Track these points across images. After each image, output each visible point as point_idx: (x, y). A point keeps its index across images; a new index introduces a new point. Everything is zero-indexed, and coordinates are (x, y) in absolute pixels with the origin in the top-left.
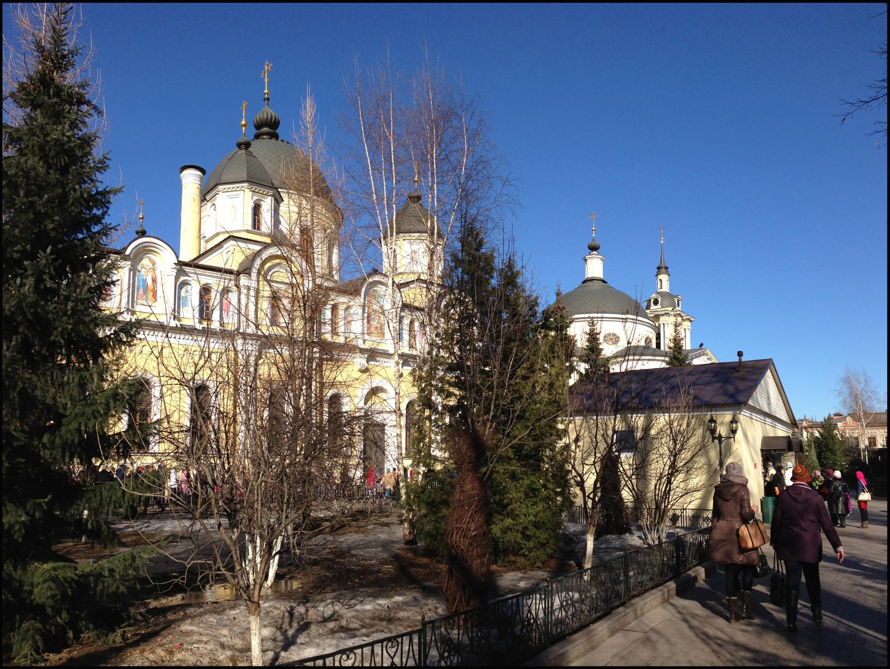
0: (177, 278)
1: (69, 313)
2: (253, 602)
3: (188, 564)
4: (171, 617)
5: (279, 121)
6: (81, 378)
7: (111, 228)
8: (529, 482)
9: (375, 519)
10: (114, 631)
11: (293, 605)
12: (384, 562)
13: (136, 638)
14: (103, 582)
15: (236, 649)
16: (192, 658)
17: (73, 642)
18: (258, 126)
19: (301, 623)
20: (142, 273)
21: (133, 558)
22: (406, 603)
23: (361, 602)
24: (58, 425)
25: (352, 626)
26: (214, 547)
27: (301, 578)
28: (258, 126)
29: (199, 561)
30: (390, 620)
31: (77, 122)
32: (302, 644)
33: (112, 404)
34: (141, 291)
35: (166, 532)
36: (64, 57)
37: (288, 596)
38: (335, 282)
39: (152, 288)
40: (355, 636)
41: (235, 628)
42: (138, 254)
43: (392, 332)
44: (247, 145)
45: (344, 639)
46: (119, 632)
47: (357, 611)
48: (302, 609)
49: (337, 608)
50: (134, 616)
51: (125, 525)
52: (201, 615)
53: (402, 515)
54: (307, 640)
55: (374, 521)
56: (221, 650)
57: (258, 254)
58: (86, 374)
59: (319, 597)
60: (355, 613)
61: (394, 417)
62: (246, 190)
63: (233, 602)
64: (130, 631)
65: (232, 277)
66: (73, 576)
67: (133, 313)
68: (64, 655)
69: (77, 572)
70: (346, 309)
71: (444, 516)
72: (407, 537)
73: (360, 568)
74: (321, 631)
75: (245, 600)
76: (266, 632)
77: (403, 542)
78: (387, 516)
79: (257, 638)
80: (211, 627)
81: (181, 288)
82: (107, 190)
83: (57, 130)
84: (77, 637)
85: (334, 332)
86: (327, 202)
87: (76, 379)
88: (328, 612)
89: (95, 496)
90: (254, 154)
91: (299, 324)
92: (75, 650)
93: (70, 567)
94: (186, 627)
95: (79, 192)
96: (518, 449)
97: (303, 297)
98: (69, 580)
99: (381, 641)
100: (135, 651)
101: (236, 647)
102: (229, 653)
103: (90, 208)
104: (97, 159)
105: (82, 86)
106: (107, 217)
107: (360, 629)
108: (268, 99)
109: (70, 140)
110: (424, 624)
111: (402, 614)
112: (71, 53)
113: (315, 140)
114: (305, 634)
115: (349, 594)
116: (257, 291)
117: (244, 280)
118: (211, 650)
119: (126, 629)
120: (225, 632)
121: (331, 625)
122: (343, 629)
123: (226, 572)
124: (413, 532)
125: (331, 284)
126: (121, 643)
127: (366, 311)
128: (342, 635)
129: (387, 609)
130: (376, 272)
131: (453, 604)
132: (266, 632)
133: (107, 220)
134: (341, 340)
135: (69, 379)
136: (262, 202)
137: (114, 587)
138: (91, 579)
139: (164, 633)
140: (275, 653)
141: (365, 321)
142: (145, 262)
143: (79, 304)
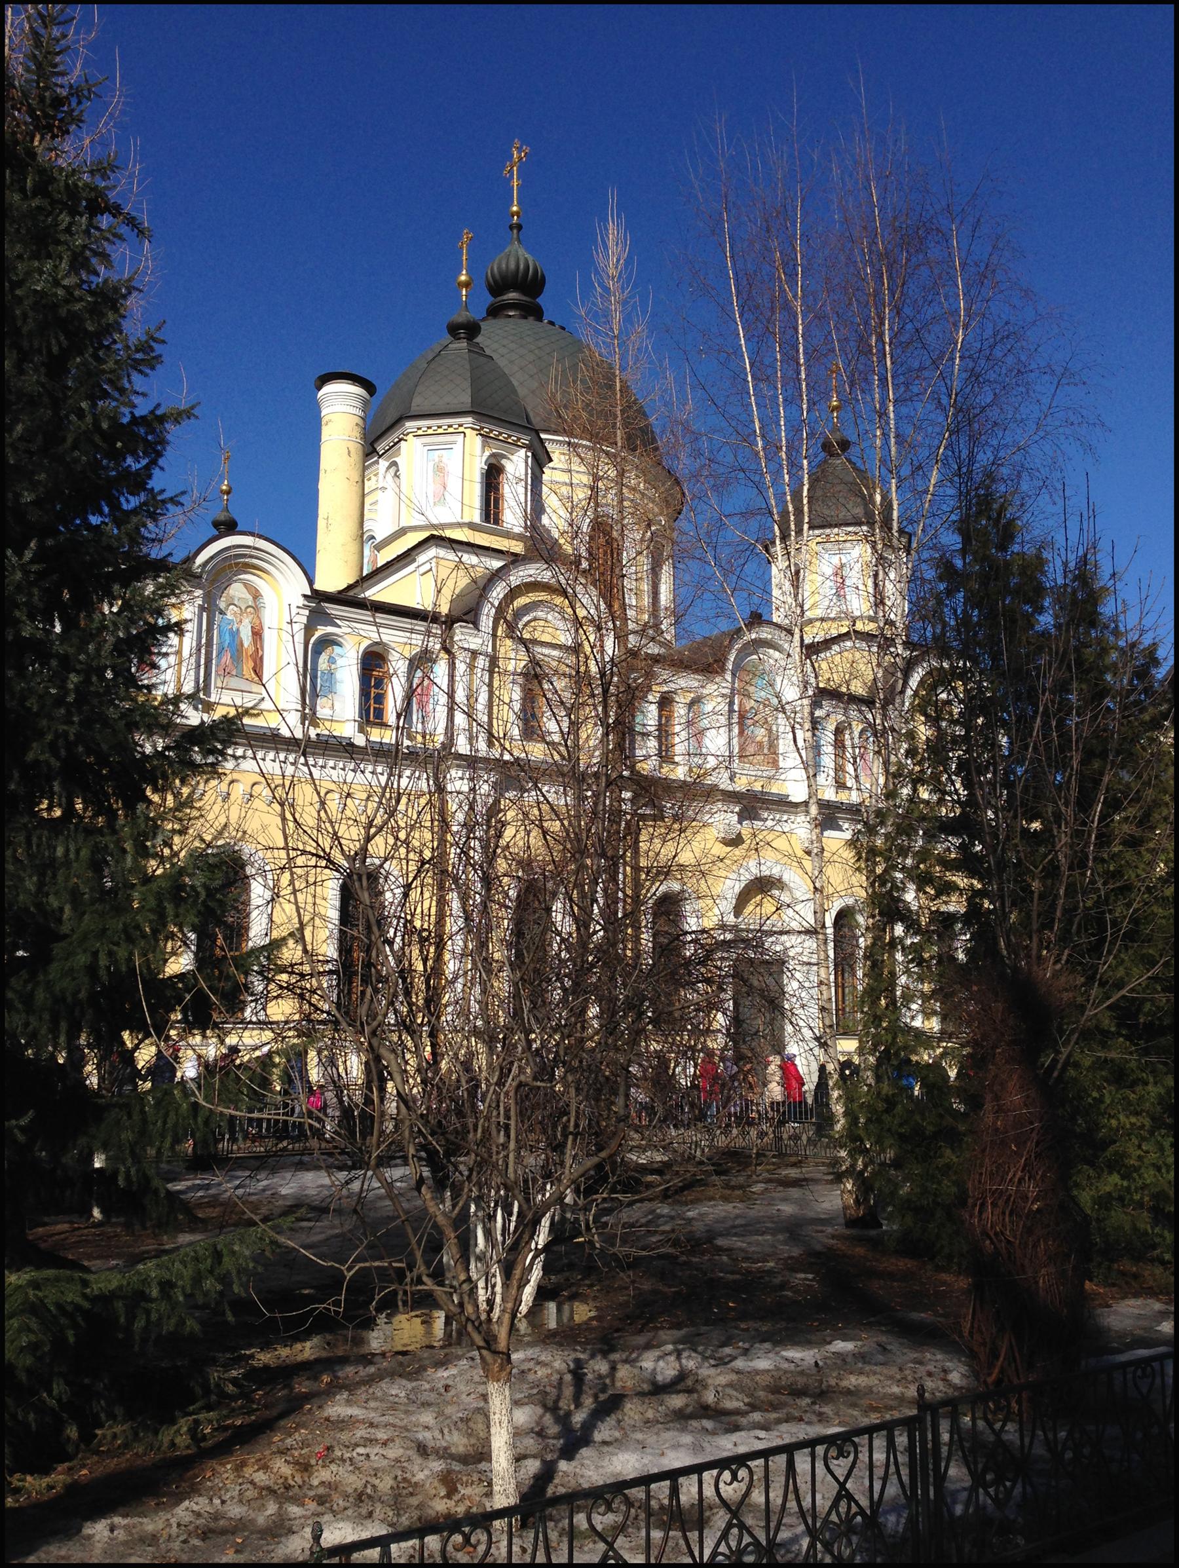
0: (309, 629)
1: (70, 699)
2: (496, 1353)
3: (349, 1269)
4: (302, 1386)
5: (543, 277)
6: (96, 849)
7: (164, 502)
8: (1163, 1091)
9: (768, 1171)
10: (173, 1421)
11: (582, 1356)
12: (793, 1265)
13: (220, 1437)
14: (148, 1312)
15: (453, 1457)
16: (353, 1478)
17: (77, 1447)
18: (498, 287)
19: (602, 1397)
20: (229, 616)
21: (218, 1256)
22: (861, 1357)
23: (746, 1352)
24: (41, 959)
25: (729, 1404)
26: (410, 1231)
27: (595, 1298)
28: (498, 287)
29: (376, 1264)
30: (823, 1395)
31: (88, 253)
32: (605, 1443)
33: (169, 908)
34: (227, 658)
35: (284, 1197)
36: (58, 102)
37: (565, 1336)
38: (666, 644)
39: (251, 651)
40: (737, 1428)
41: (449, 1410)
42: (224, 569)
43: (803, 753)
44: (471, 330)
45: (714, 1433)
46: (184, 1424)
47: (738, 1372)
48: (600, 1366)
49: (690, 1364)
50: (218, 1385)
51: (189, 1183)
52: (370, 1381)
53: (836, 1162)
54: (617, 1434)
55: (766, 1175)
56: (418, 1460)
57: (495, 576)
58: (108, 840)
59: (641, 1340)
60: (734, 1377)
61: (811, 943)
62: (468, 431)
63: (442, 1353)
64: (210, 1421)
65: (436, 629)
66: (79, 1300)
67: (209, 707)
68: (59, 1478)
69: (88, 1291)
70: (691, 705)
71: (948, 1166)
72: (852, 1212)
73: (738, 1277)
74: (650, 1414)
75: (479, 1348)
76: (523, 1416)
77: (842, 1221)
78: (794, 1165)
79: (504, 1432)
80: (394, 1407)
81: (317, 652)
82: (159, 412)
83: (41, 273)
84: (87, 1437)
85: (665, 755)
86: (647, 462)
87: (85, 853)
88: (667, 1370)
89: (130, 1116)
90: (488, 352)
91: (591, 734)
92: (83, 1466)
93: (70, 1280)
94: (337, 1409)
95: (89, 419)
96: (1126, 1012)
97: (602, 674)
98: (69, 1308)
99: (811, 1443)
100: (224, 1465)
101: (453, 1450)
102: (437, 1466)
103: (119, 456)
104: (132, 341)
105: (101, 170)
106: (156, 472)
107: (747, 1413)
108: (519, 227)
109: (71, 294)
110: (922, 1404)
111: (852, 1381)
112: (76, 92)
113: (627, 319)
114: (611, 1421)
115: (716, 1335)
116: (494, 660)
117: (464, 637)
118: (397, 1461)
119: (201, 1416)
120: (427, 1417)
121: (677, 1401)
122: (706, 1411)
123: (436, 1288)
124: (866, 1200)
125: (654, 649)
126: (188, 1447)
127: (736, 708)
128: (708, 1424)
129: (814, 1371)
130: (757, 619)
131: (991, 1366)
132: (523, 1416)
133: (157, 482)
134: (680, 773)
135: (67, 851)
136: (504, 462)
137: (173, 1321)
138: (119, 1305)
139: (288, 1423)
140: (544, 1462)
141: (736, 730)
142: (236, 590)
143: (94, 679)
